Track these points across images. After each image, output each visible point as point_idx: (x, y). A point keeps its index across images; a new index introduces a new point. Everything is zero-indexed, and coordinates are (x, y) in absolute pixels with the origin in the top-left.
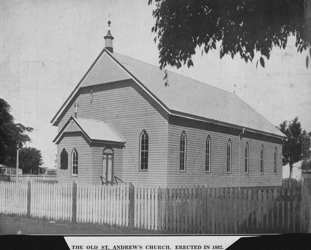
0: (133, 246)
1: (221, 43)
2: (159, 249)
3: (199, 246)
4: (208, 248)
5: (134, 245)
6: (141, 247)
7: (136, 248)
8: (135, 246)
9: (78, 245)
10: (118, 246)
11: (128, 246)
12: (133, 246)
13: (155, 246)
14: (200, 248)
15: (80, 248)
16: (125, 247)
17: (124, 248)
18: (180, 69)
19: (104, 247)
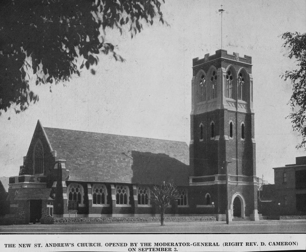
0: (27, 244)
1: (102, 27)
2: (90, 246)
3: (124, 243)
4: (295, 243)
5: (66, 243)
6: (36, 245)
7: (30, 247)
8: (29, 244)
9: (10, 243)
10: (50, 244)
11: (248, 243)
12: (27, 244)
13: (86, 244)
14: (126, 245)
15: (12, 246)
16: (57, 244)
17: (162, 245)
19: (37, 245)
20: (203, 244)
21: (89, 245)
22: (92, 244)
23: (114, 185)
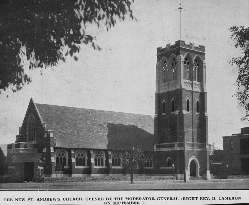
0: (22, 199)
2: (73, 200)
3: (101, 198)
4: (240, 197)
5: (54, 197)
6: (29, 200)
7: (24, 201)
8: (24, 199)
9: (8, 198)
10: (41, 198)
11: (202, 198)
12: (22, 199)
13: (70, 198)
14: (102, 199)
15: (10, 200)
16: (46, 199)
17: (132, 199)
18: (7, 98)
19: (30, 199)
20: (165, 199)
21: (72, 200)
22: (75, 198)
23: (92, 151)
